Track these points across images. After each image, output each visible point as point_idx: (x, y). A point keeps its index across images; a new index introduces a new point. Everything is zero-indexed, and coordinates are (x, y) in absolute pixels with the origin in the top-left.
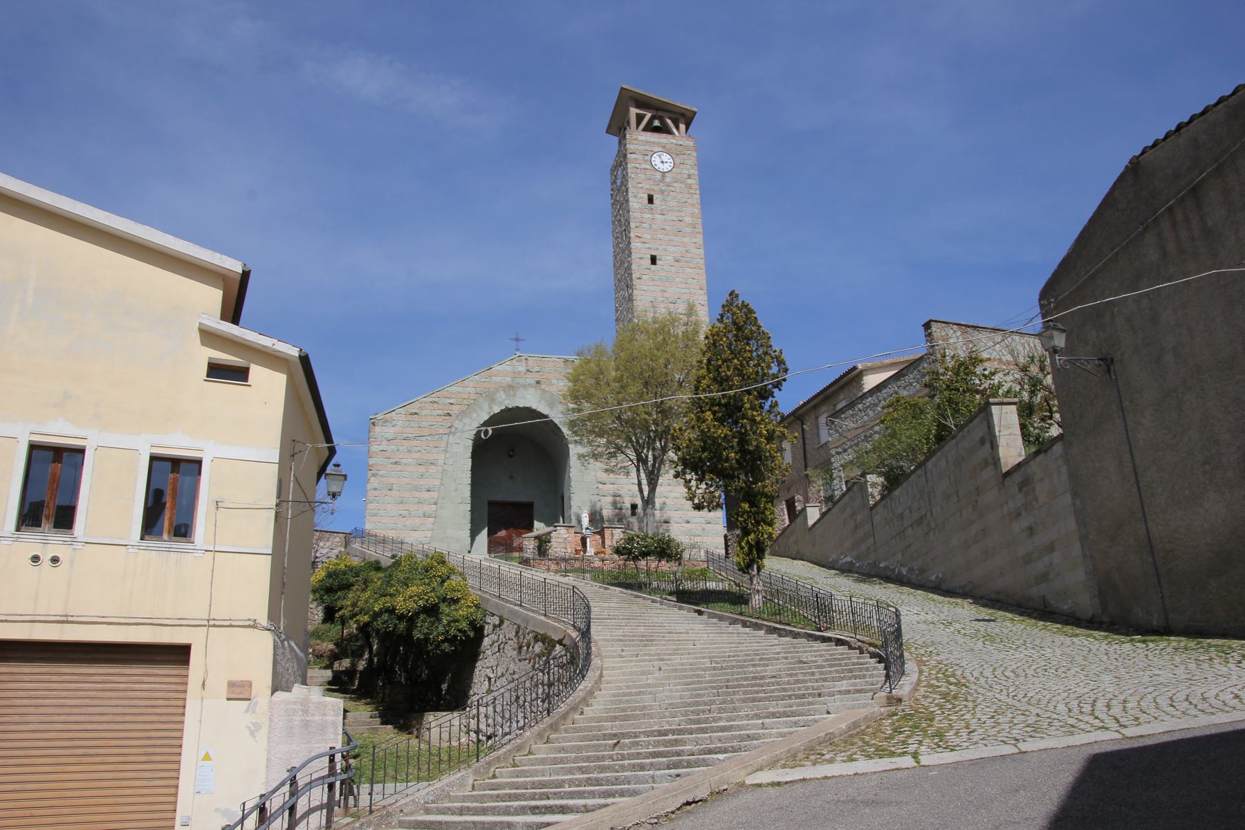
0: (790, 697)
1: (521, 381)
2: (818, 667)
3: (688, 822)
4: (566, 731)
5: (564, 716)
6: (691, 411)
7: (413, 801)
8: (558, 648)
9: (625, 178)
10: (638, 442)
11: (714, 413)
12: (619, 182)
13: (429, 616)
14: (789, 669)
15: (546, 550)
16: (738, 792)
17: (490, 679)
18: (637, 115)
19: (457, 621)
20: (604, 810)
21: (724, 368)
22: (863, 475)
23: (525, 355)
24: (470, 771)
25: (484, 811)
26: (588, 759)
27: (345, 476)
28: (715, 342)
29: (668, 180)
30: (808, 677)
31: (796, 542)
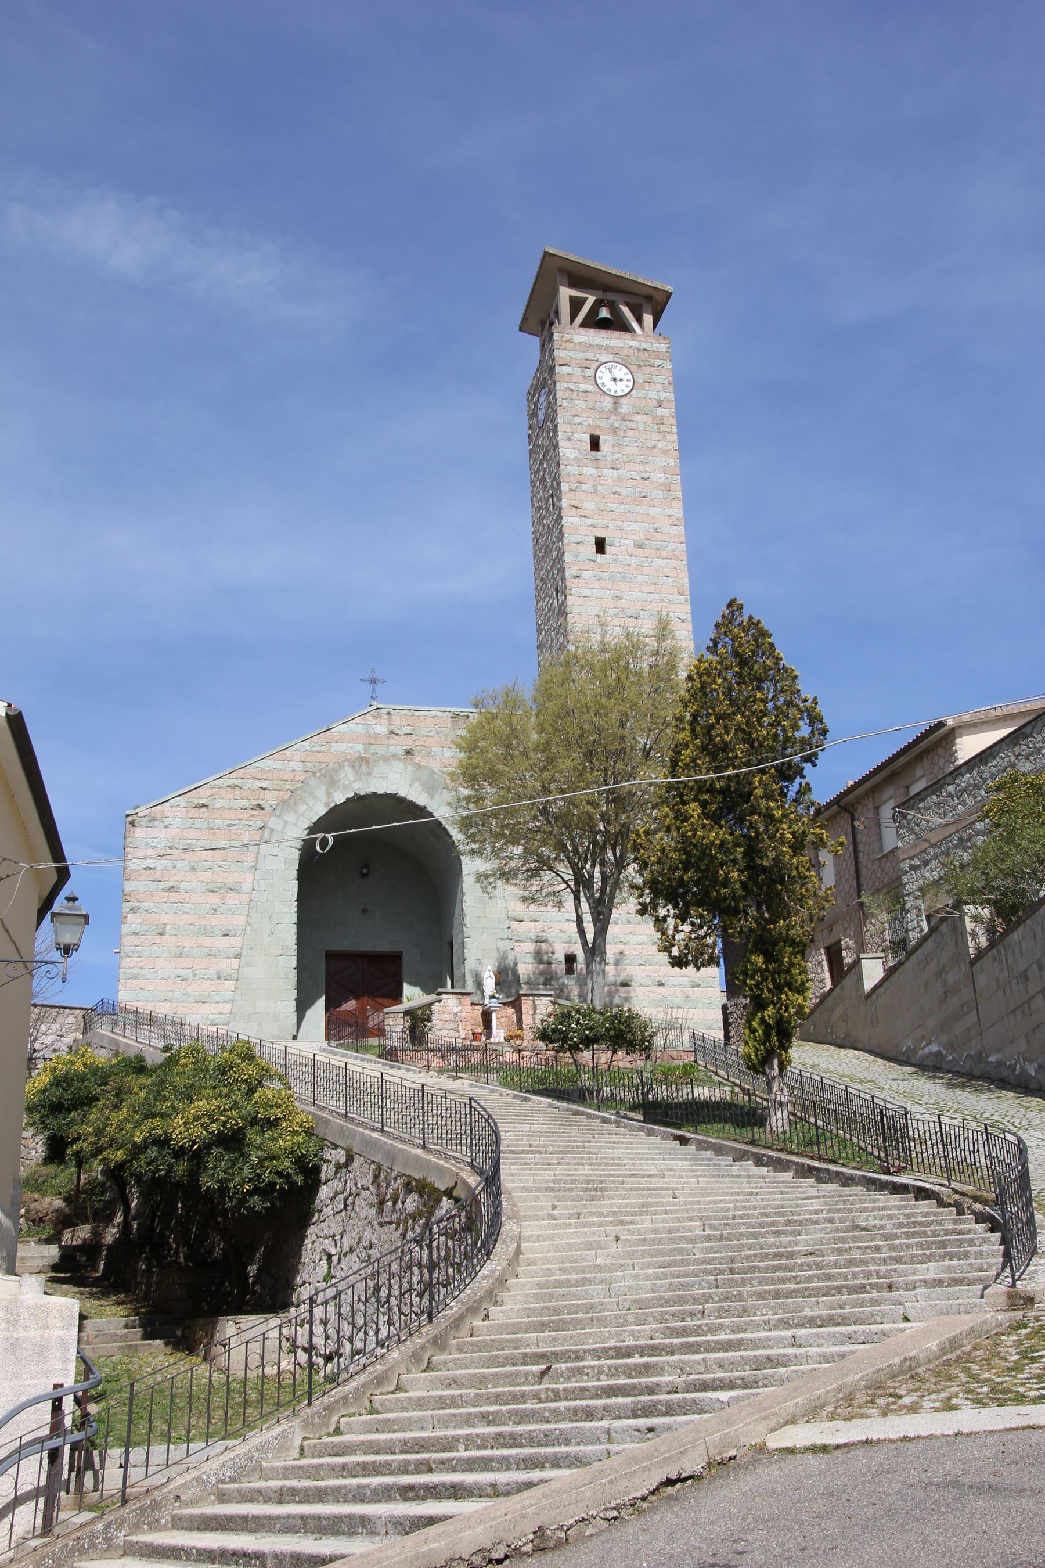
0: (839, 1290)
1: (381, 750)
2: (887, 1237)
3: (669, 1516)
4: (460, 1350)
5: (457, 1323)
6: (664, 801)
7: (198, 1479)
8: (446, 1203)
9: (552, 407)
10: (575, 850)
11: (704, 805)
12: (541, 415)
13: (227, 1149)
14: (836, 1240)
15: (423, 1034)
16: (754, 1462)
17: (330, 1256)
18: (572, 299)
19: (274, 1158)
20: (526, 1494)
21: (719, 730)
22: (958, 905)
23: (388, 707)
24: (296, 1422)
25: (320, 1496)
26: (497, 1399)
27: (86, 918)
28: (704, 685)
29: (624, 409)
30: (869, 1255)
31: (844, 1018)
